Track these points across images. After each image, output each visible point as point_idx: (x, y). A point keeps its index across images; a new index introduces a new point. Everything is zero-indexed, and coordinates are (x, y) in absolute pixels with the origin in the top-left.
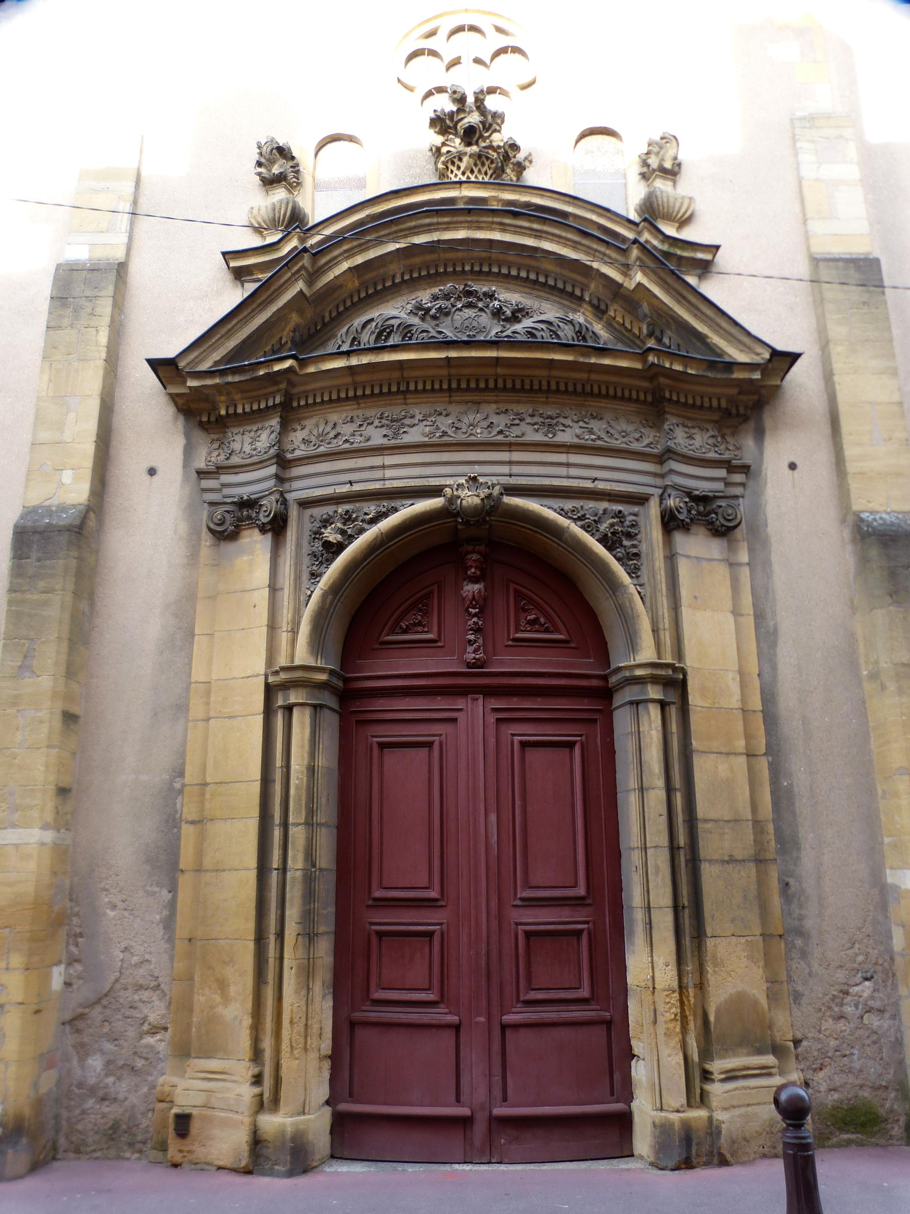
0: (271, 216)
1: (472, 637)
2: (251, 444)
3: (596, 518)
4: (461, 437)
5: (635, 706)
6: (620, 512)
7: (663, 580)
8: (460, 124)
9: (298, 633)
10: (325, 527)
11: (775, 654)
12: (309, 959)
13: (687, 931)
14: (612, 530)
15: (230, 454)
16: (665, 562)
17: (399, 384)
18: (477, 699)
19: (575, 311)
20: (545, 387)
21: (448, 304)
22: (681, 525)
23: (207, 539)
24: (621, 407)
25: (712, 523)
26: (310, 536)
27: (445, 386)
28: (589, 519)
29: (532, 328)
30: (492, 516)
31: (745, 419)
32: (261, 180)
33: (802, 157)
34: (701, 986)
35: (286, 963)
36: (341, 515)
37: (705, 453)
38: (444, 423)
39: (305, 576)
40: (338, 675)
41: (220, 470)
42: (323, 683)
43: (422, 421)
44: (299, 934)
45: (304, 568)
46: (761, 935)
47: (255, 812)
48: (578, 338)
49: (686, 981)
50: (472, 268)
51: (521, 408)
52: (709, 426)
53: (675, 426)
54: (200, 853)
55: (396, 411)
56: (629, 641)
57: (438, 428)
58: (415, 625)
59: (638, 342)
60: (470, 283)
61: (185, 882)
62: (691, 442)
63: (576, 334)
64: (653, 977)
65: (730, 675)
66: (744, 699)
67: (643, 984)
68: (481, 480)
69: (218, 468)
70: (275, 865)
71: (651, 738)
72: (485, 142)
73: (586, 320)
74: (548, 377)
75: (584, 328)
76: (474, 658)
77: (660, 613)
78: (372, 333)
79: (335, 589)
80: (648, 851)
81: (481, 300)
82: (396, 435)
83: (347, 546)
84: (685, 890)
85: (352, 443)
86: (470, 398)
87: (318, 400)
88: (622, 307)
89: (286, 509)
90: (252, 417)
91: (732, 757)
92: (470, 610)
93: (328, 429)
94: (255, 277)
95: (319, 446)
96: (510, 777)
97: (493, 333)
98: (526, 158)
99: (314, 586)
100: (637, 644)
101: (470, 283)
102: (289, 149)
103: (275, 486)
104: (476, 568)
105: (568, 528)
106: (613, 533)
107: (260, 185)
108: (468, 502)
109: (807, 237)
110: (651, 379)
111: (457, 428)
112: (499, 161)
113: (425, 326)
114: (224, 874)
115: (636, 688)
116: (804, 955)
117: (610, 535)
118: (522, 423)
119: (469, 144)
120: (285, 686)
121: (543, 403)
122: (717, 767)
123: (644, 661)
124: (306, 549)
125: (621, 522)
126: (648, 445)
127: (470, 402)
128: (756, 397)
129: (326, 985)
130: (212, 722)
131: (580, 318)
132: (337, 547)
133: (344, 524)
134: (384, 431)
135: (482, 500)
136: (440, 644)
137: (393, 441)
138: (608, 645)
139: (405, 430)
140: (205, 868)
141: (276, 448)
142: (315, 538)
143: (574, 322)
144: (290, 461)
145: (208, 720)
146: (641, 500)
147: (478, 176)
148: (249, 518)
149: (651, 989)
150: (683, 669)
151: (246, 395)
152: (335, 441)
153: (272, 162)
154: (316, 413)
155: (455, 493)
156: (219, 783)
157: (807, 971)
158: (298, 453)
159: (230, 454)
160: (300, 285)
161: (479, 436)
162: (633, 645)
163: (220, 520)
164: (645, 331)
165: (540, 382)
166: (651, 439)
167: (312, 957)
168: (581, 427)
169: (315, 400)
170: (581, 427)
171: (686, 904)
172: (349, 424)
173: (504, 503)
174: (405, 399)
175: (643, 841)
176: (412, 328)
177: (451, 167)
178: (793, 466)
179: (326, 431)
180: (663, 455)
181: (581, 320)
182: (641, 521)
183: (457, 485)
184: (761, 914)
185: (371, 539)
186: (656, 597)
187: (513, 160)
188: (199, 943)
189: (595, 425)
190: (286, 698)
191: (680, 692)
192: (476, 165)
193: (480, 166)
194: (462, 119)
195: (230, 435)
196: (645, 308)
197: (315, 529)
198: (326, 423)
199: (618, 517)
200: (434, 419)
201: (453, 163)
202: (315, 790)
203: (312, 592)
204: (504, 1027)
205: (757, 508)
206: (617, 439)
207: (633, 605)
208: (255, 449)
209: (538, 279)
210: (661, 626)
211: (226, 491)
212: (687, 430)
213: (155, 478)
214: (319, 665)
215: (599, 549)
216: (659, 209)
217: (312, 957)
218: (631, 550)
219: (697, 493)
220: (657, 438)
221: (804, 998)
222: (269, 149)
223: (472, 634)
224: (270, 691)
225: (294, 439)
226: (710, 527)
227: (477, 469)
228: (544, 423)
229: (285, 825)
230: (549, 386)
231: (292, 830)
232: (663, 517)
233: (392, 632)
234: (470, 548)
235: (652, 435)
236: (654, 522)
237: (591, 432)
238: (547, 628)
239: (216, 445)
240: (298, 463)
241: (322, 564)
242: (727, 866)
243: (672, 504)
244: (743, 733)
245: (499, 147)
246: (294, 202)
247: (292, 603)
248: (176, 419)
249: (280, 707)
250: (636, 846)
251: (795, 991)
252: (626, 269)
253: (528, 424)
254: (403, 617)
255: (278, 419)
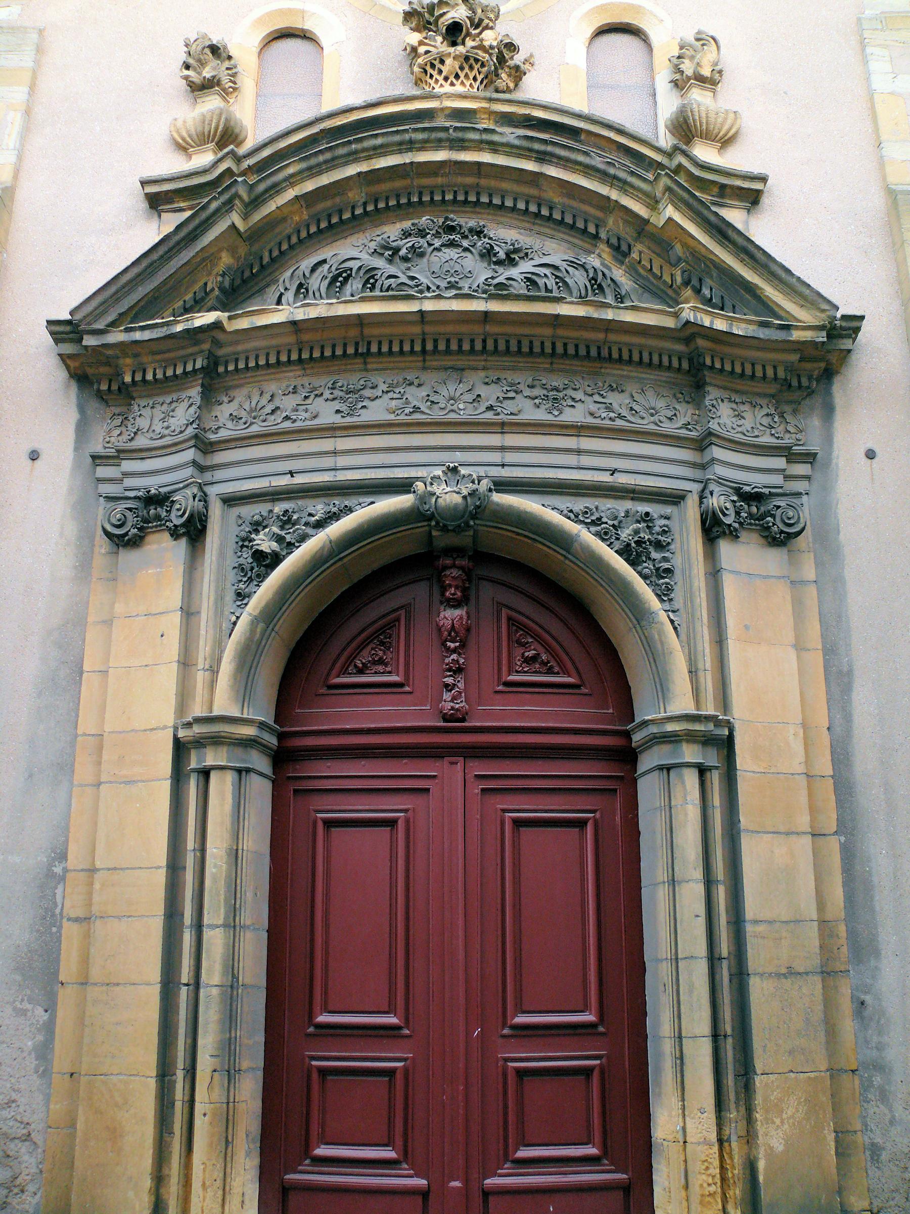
0: (200, 129)
1: (450, 680)
2: (163, 420)
3: (616, 523)
4: (437, 414)
5: (665, 771)
6: (647, 514)
7: (704, 604)
8: (442, 20)
9: (218, 672)
10: (257, 531)
11: (849, 701)
12: (228, 1103)
13: (730, 1067)
14: (636, 539)
15: (135, 433)
16: (706, 578)
17: (357, 344)
18: (456, 763)
19: (590, 252)
20: (548, 350)
21: (423, 242)
22: (727, 532)
23: (102, 545)
24: (648, 376)
25: (768, 528)
26: (237, 543)
27: (418, 348)
28: (606, 523)
29: (533, 273)
30: (477, 518)
31: (811, 393)
32: (188, 85)
33: (873, 66)
34: (750, 1137)
35: (199, 1108)
36: (278, 517)
37: (757, 436)
38: (416, 396)
39: (230, 596)
40: (270, 728)
41: (121, 454)
42: (251, 740)
43: (387, 392)
44: (215, 1071)
45: (229, 585)
46: (828, 1070)
47: (160, 909)
48: (592, 286)
49: (727, 1133)
50: (455, 197)
51: (516, 377)
52: (763, 402)
53: (719, 401)
54: (85, 960)
55: (354, 379)
56: (658, 687)
57: (407, 402)
58: (375, 663)
59: (670, 292)
60: (452, 216)
61: (66, 998)
62: (740, 423)
63: (590, 281)
64: (684, 1129)
65: (791, 729)
66: (808, 761)
67: (670, 1137)
68: (463, 471)
69: (118, 451)
70: (184, 980)
71: (686, 815)
72: (474, 40)
73: (603, 264)
74: (553, 336)
75: (600, 274)
76: (452, 708)
77: (700, 648)
78: (325, 277)
79: (269, 615)
80: (680, 964)
81: (466, 237)
82: (352, 412)
83: (284, 557)
84: (727, 1013)
85: (294, 421)
86: (450, 364)
87: (252, 364)
88: (649, 248)
89: (206, 508)
90: (165, 385)
91: (794, 838)
92: (449, 644)
93: (264, 401)
94: (176, 205)
95: (252, 424)
96: (499, 867)
97: (481, 279)
98: (526, 61)
99: (240, 610)
100: (668, 690)
101: (452, 216)
102: (225, 47)
103: (193, 477)
104: (457, 587)
105: (578, 535)
106: (638, 543)
107: (187, 91)
108: (445, 500)
109: (881, 164)
110: (688, 340)
111: (432, 402)
112: (492, 63)
113: (392, 270)
114: (117, 989)
115: (666, 748)
116: (884, 1096)
117: (633, 545)
118: (519, 397)
119: (454, 44)
120: (200, 743)
121: (545, 370)
122: (772, 852)
123: (678, 712)
124: (231, 560)
125: (648, 527)
126: (686, 426)
127: (451, 368)
128: (823, 365)
129: (250, 1138)
130: (102, 787)
131: (593, 261)
132: (272, 559)
133: (282, 528)
134: (337, 405)
135: (465, 497)
136: (407, 689)
137: (349, 419)
138: (632, 691)
139: (364, 404)
140: (92, 981)
141: (195, 426)
142: (242, 546)
143: (587, 267)
144: (212, 444)
145: (99, 784)
146: (676, 499)
147: (465, 81)
148: (158, 518)
149: (682, 1143)
150: (728, 722)
151: (158, 357)
152: (273, 417)
153: (202, 63)
154: (247, 381)
155: (429, 488)
156: (112, 869)
157: (889, 1117)
158: (223, 434)
159: (135, 433)
160: (235, 218)
161: (462, 413)
162: (662, 688)
163: (119, 520)
164: (679, 279)
165: (542, 343)
166: (688, 419)
167: (232, 1100)
168: (595, 402)
169: (247, 364)
170: (595, 402)
171: (729, 1032)
172: (291, 395)
173: (492, 502)
174: (365, 363)
175: (673, 951)
176: (375, 272)
177: (430, 70)
178: (871, 455)
179: (260, 406)
180: (703, 440)
181: (597, 263)
182: (674, 525)
183: (432, 478)
184: (827, 1042)
185: (315, 550)
186: (694, 628)
187: (511, 63)
188: (84, 1079)
189: (614, 399)
190: (201, 759)
191: (725, 752)
192: (462, 68)
193: (467, 70)
194: (444, 13)
195: (136, 408)
196: (678, 249)
197: (243, 534)
198: (261, 395)
199: (645, 521)
200: (402, 391)
201: (433, 66)
202: (239, 881)
203: (238, 618)
204: (486, 1194)
205: (825, 509)
206: (643, 418)
207: (663, 638)
208: (167, 428)
209: (540, 211)
210: (700, 666)
211: (129, 482)
212: (734, 406)
213: (37, 462)
214: (245, 716)
215: (619, 564)
216: (695, 125)
217: (232, 1100)
218: (662, 564)
219: (747, 489)
220: (696, 417)
221: (884, 1153)
222: (200, 48)
223: (451, 676)
224: (180, 749)
225: (218, 414)
226: (766, 534)
227: (459, 456)
228: (547, 396)
229: (199, 927)
230: (554, 348)
231: (207, 934)
232: (703, 522)
233: (344, 672)
234: (448, 562)
235: (690, 412)
236: (692, 528)
237: (609, 408)
238: (552, 667)
239: (118, 422)
240: (223, 446)
241: (252, 580)
242: (784, 980)
243: (715, 505)
244: (807, 807)
245: (492, 47)
246: (227, 111)
247: (211, 632)
248: (67, 386)
249: (194, 770)
250: (664, 957)
251: (873, 1144)
252: (653, 203)
253: (526, 397)
254: (358, 653)
255: (199, 389)
